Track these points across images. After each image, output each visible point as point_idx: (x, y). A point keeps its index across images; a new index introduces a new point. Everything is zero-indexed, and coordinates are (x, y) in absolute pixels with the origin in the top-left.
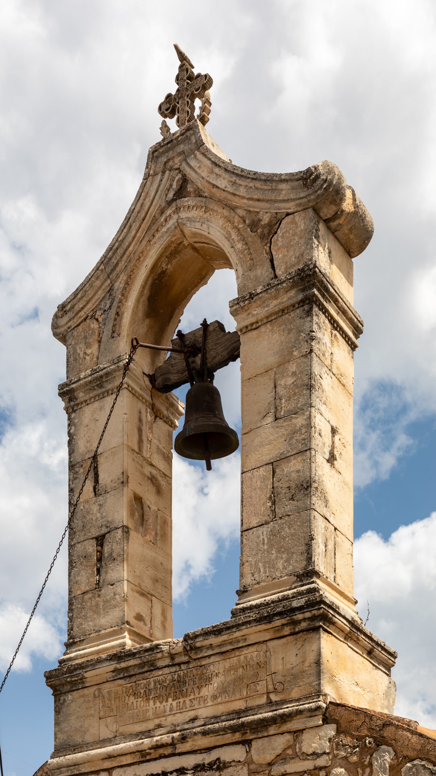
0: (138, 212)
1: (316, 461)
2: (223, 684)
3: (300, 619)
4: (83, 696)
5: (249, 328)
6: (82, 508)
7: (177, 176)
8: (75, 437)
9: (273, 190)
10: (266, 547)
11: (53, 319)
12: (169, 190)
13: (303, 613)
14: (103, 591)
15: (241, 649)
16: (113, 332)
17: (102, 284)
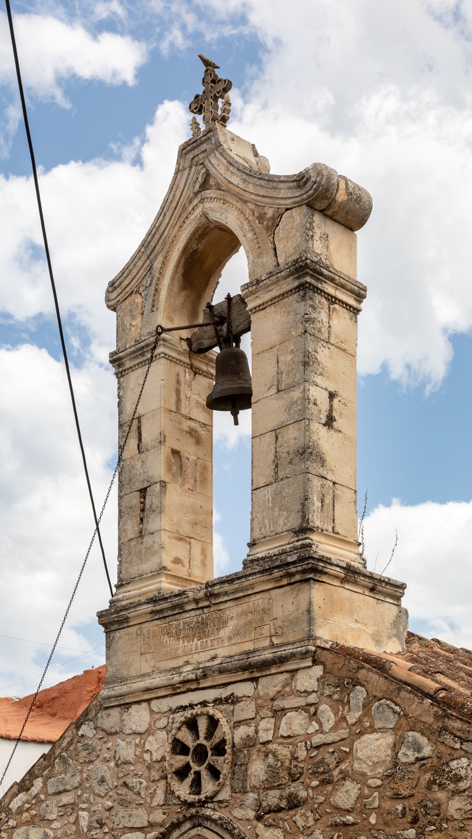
0: (171, 202)
1: (310, 429)
2: (237, 627)
4: (128, 634)
5: (258, 309)
6: (128, 463)
7: (202, 170)
8: (123, 399)
9: (275, 188)
10: (270, 505)
11: (106, 293)
12: (195, 182)
13: (296, 567)
14: (145, 539)
15: (250, 597)
16: (153, 306)
17: (144, 264)
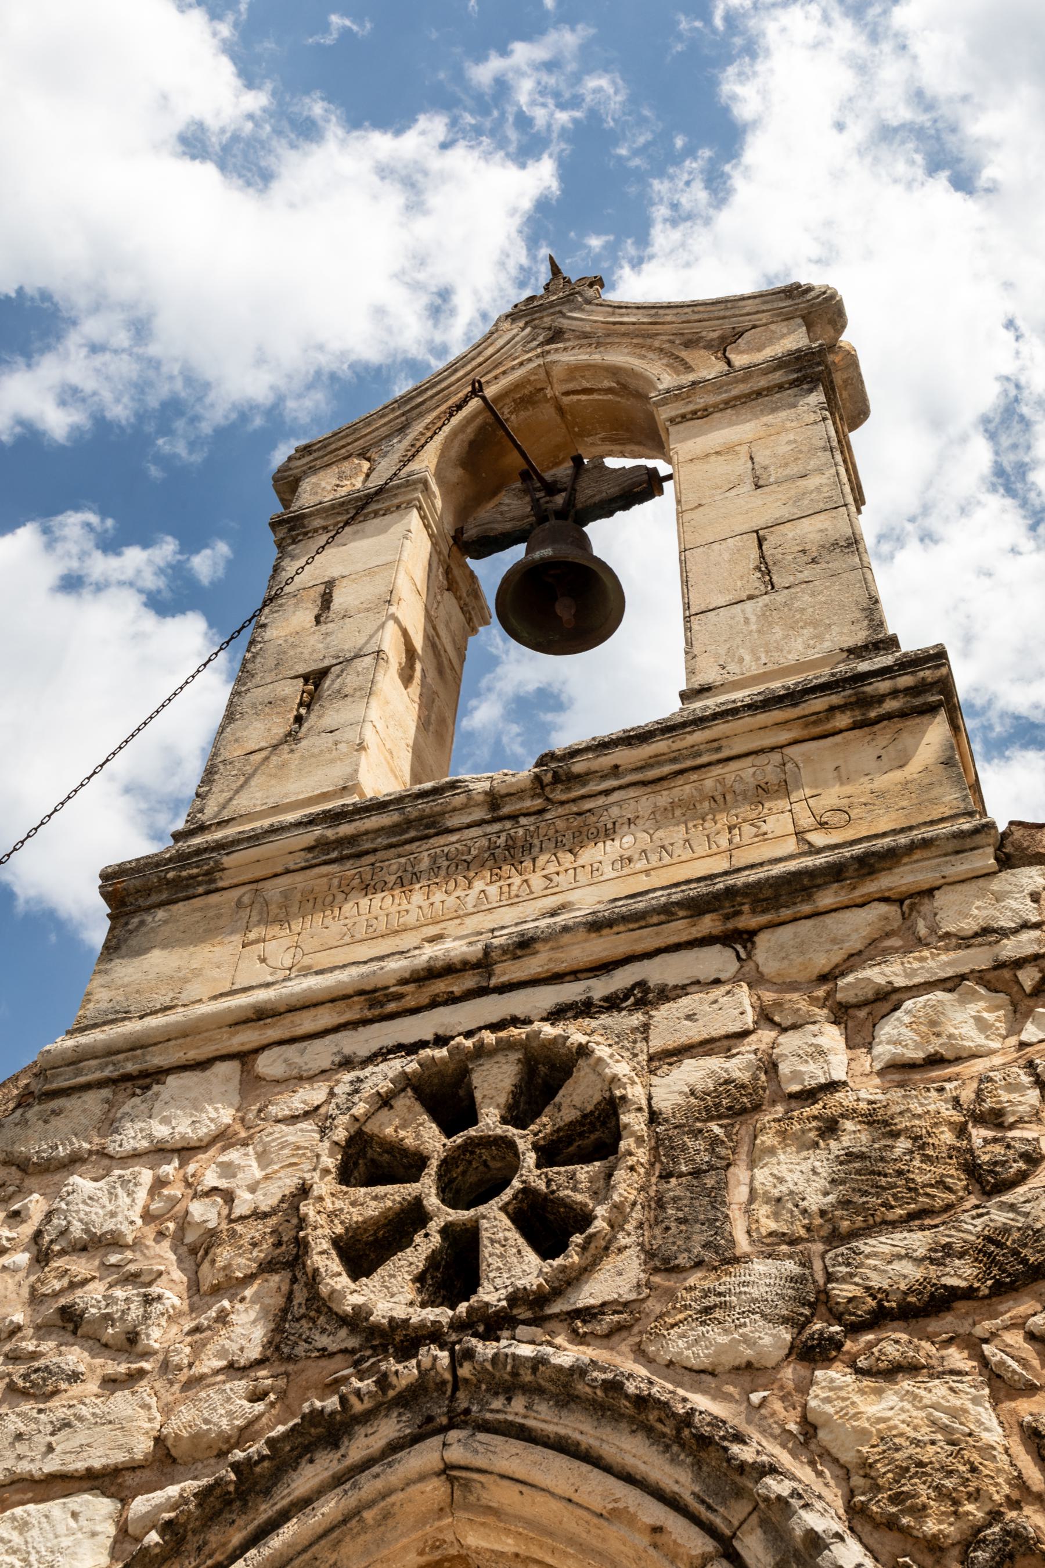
3: (881, 692)
